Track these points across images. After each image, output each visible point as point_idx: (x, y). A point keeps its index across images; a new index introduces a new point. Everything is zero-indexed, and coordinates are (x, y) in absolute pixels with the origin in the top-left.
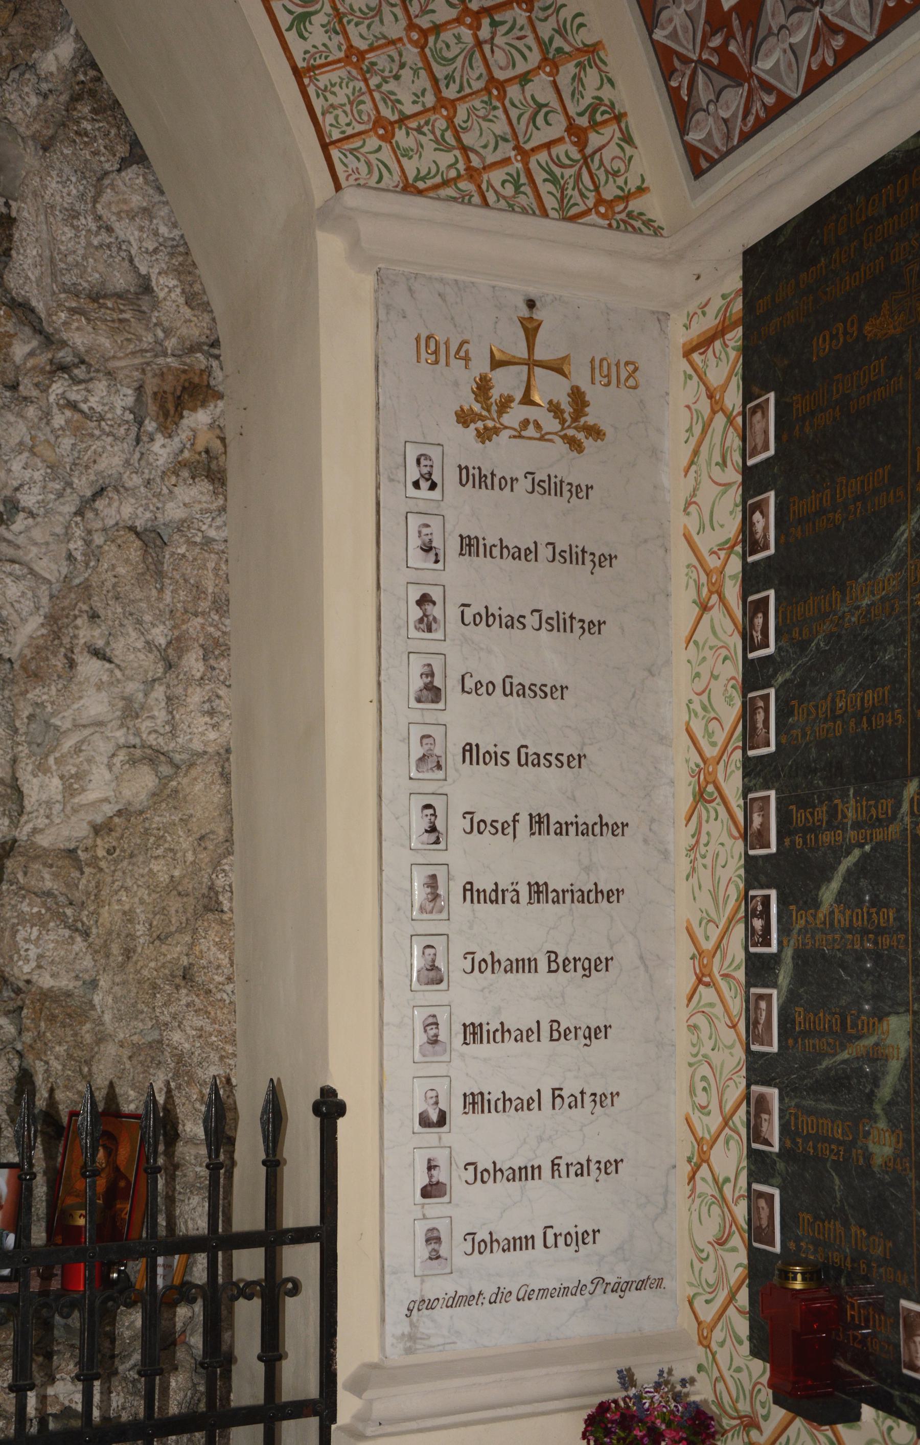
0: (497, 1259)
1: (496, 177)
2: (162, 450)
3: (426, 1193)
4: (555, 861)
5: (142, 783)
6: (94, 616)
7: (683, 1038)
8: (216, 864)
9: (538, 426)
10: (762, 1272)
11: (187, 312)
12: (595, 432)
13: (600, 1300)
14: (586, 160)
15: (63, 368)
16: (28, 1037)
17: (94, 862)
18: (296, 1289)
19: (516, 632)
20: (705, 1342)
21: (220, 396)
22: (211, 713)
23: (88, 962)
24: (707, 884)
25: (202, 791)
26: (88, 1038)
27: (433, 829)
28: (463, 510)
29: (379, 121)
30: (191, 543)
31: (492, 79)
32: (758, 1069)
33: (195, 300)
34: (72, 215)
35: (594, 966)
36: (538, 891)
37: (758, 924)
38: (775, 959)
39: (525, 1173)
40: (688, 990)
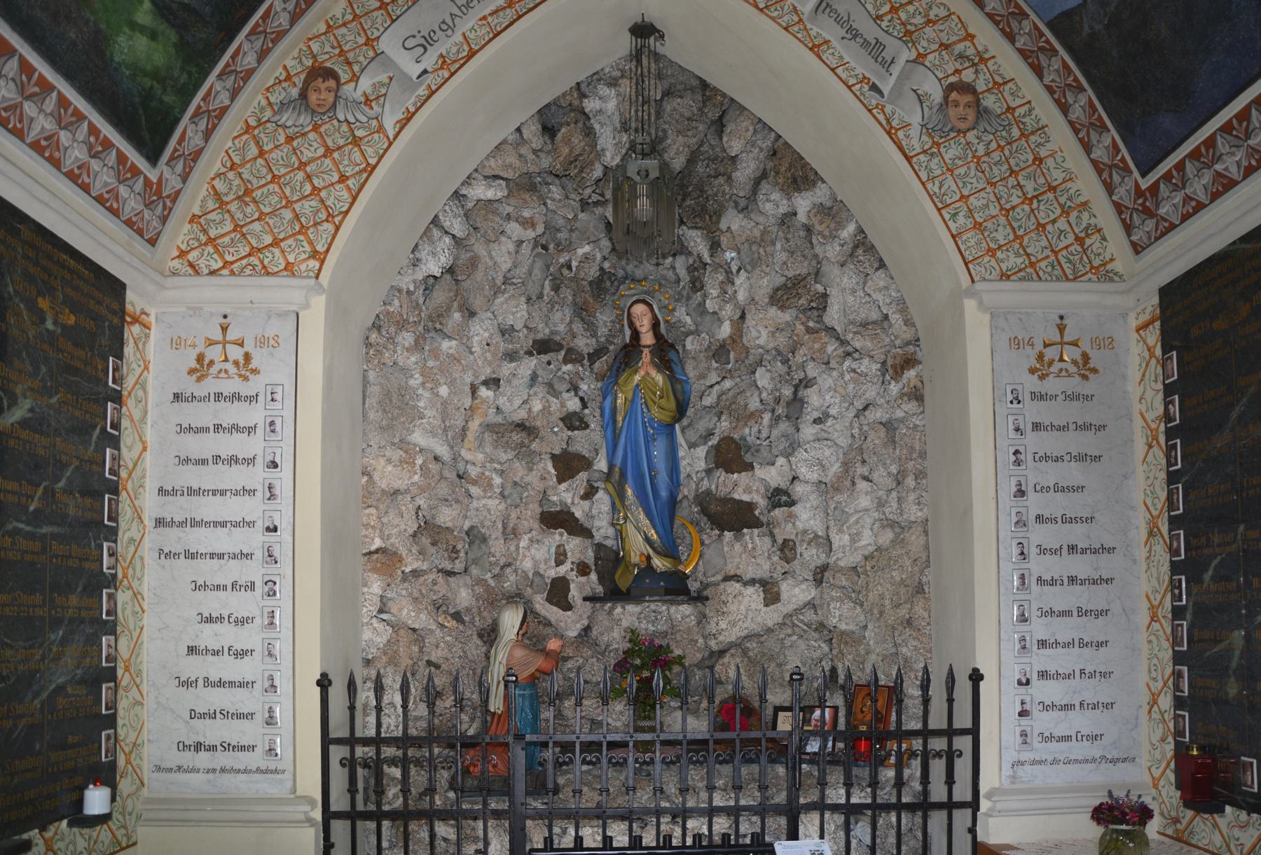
0: (1054, 745)
1: (1043, 264)
2: (894, 388)
3: (1021, 714)
4: (1081, 566)
5: (888, 535)
6: (864, 462)
7: (1145, 647)
8: (922, 572)
9: (1067, 371)
10: (1181, 753)
11: (905, 328)
12: (1095, 371)
13: (1103, 766)
14: (1085, 251)
15: (849, 354)
16: (835, 652)
17: (865, 573)
19: (1059, 464)
21: (920, 363)
22: (919, 504)
23: (862, 618)
24: (1155, 575)
25: (915, 539)
26: (862, 652)
27: (1022, 553)
28: (1032, 411)
29: (989, 250)
31: (1039, 224)
32: (1178, 658)
34: (854, 291)
35: (1100, 613)
36: (1072, 580)
37: (1177, 591)
38: (1185, 607)
39: (1067, 707)
40: (1147, 623)
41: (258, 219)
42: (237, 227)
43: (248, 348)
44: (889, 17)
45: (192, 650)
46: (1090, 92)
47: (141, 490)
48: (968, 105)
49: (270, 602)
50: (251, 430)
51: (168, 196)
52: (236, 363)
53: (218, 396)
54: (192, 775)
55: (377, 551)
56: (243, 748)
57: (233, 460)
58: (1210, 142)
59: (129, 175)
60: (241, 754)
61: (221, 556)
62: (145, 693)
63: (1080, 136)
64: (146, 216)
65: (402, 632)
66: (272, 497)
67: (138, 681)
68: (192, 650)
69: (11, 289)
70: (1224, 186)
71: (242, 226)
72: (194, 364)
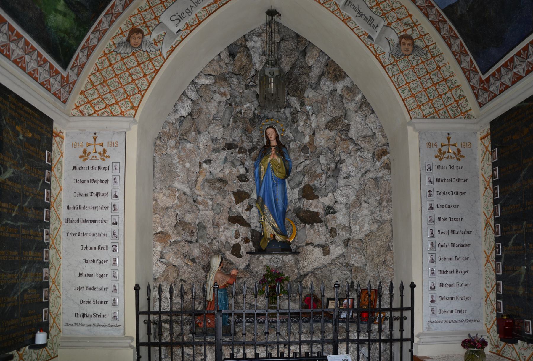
0: (445, 315)
1: (441, 112)
2: (378, 164)
3: (431, 302)
4: (457, 239)
5: (376, 226)
6: (365, 195)
7: (484, 273)
8: (390, 242)
9: (451, 156)
10: (499, 318)
11: (382, 138)
12: (463, 156)
13: (466, 323)
15: (359, 150)
17: (366, 242)
18: (406, 319)
19: (448, 196)
20: (488, 332)
21: (389, 153)
22: (388, 213)
24: (488, 243)
25: (387, 228)
26: (365, 275)
27: (432, 234)
28: (436, 174)
29: (418, 105)
30: (384, 181)
32: (498, 278)
33: (384, 136)
34: (361, 123)
35: (466, 259)
36: (453, 245)
37: (497, 250)
38: (501, 256)
39: (451, 299)
41: (109, 93)
42: (100, 96)
43: (105, 147)
44: (376, 7)
45: (81, 274)
46: (461, 39)
47: (60, 207)
48: (409, 44)
49: (114, 254)
50: (106, 182)
51: (71, 83)
52: (100, 153)
53: (92, 167)
54: (81, 327)
55: (159, 233)
56: (103, 316)
57: (99, 194)
58: (512, 60)
59: (54, 74)
60: (102, 318)
61: (93, 235)
62: (61, 293)
63: (457, 57)
64: (62, 91)
65: (170, 267)
66: (115, 210)
67: (58, 287)
68: (81, 274)
69: (5, 122)
70: (517, 78)
71: (102, 96)
72: (82, 154)
